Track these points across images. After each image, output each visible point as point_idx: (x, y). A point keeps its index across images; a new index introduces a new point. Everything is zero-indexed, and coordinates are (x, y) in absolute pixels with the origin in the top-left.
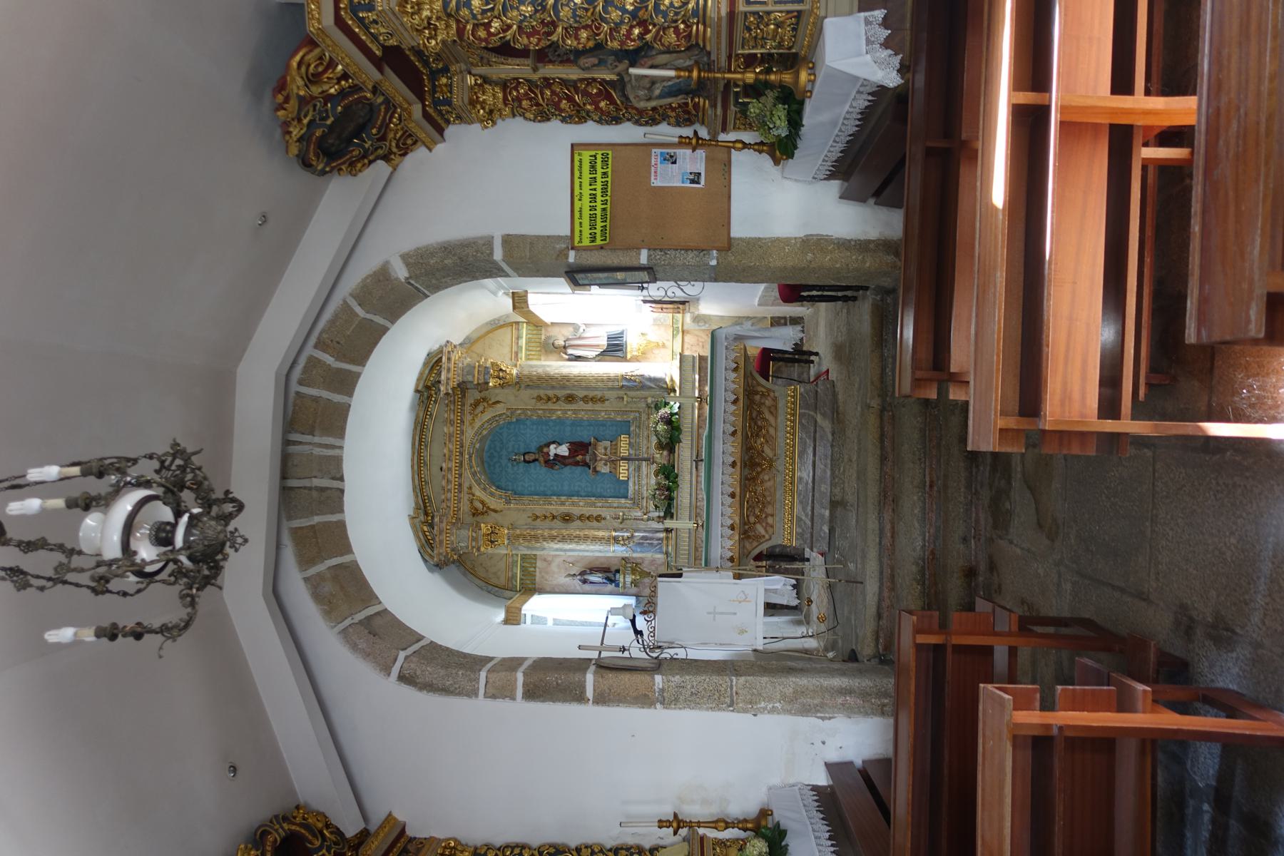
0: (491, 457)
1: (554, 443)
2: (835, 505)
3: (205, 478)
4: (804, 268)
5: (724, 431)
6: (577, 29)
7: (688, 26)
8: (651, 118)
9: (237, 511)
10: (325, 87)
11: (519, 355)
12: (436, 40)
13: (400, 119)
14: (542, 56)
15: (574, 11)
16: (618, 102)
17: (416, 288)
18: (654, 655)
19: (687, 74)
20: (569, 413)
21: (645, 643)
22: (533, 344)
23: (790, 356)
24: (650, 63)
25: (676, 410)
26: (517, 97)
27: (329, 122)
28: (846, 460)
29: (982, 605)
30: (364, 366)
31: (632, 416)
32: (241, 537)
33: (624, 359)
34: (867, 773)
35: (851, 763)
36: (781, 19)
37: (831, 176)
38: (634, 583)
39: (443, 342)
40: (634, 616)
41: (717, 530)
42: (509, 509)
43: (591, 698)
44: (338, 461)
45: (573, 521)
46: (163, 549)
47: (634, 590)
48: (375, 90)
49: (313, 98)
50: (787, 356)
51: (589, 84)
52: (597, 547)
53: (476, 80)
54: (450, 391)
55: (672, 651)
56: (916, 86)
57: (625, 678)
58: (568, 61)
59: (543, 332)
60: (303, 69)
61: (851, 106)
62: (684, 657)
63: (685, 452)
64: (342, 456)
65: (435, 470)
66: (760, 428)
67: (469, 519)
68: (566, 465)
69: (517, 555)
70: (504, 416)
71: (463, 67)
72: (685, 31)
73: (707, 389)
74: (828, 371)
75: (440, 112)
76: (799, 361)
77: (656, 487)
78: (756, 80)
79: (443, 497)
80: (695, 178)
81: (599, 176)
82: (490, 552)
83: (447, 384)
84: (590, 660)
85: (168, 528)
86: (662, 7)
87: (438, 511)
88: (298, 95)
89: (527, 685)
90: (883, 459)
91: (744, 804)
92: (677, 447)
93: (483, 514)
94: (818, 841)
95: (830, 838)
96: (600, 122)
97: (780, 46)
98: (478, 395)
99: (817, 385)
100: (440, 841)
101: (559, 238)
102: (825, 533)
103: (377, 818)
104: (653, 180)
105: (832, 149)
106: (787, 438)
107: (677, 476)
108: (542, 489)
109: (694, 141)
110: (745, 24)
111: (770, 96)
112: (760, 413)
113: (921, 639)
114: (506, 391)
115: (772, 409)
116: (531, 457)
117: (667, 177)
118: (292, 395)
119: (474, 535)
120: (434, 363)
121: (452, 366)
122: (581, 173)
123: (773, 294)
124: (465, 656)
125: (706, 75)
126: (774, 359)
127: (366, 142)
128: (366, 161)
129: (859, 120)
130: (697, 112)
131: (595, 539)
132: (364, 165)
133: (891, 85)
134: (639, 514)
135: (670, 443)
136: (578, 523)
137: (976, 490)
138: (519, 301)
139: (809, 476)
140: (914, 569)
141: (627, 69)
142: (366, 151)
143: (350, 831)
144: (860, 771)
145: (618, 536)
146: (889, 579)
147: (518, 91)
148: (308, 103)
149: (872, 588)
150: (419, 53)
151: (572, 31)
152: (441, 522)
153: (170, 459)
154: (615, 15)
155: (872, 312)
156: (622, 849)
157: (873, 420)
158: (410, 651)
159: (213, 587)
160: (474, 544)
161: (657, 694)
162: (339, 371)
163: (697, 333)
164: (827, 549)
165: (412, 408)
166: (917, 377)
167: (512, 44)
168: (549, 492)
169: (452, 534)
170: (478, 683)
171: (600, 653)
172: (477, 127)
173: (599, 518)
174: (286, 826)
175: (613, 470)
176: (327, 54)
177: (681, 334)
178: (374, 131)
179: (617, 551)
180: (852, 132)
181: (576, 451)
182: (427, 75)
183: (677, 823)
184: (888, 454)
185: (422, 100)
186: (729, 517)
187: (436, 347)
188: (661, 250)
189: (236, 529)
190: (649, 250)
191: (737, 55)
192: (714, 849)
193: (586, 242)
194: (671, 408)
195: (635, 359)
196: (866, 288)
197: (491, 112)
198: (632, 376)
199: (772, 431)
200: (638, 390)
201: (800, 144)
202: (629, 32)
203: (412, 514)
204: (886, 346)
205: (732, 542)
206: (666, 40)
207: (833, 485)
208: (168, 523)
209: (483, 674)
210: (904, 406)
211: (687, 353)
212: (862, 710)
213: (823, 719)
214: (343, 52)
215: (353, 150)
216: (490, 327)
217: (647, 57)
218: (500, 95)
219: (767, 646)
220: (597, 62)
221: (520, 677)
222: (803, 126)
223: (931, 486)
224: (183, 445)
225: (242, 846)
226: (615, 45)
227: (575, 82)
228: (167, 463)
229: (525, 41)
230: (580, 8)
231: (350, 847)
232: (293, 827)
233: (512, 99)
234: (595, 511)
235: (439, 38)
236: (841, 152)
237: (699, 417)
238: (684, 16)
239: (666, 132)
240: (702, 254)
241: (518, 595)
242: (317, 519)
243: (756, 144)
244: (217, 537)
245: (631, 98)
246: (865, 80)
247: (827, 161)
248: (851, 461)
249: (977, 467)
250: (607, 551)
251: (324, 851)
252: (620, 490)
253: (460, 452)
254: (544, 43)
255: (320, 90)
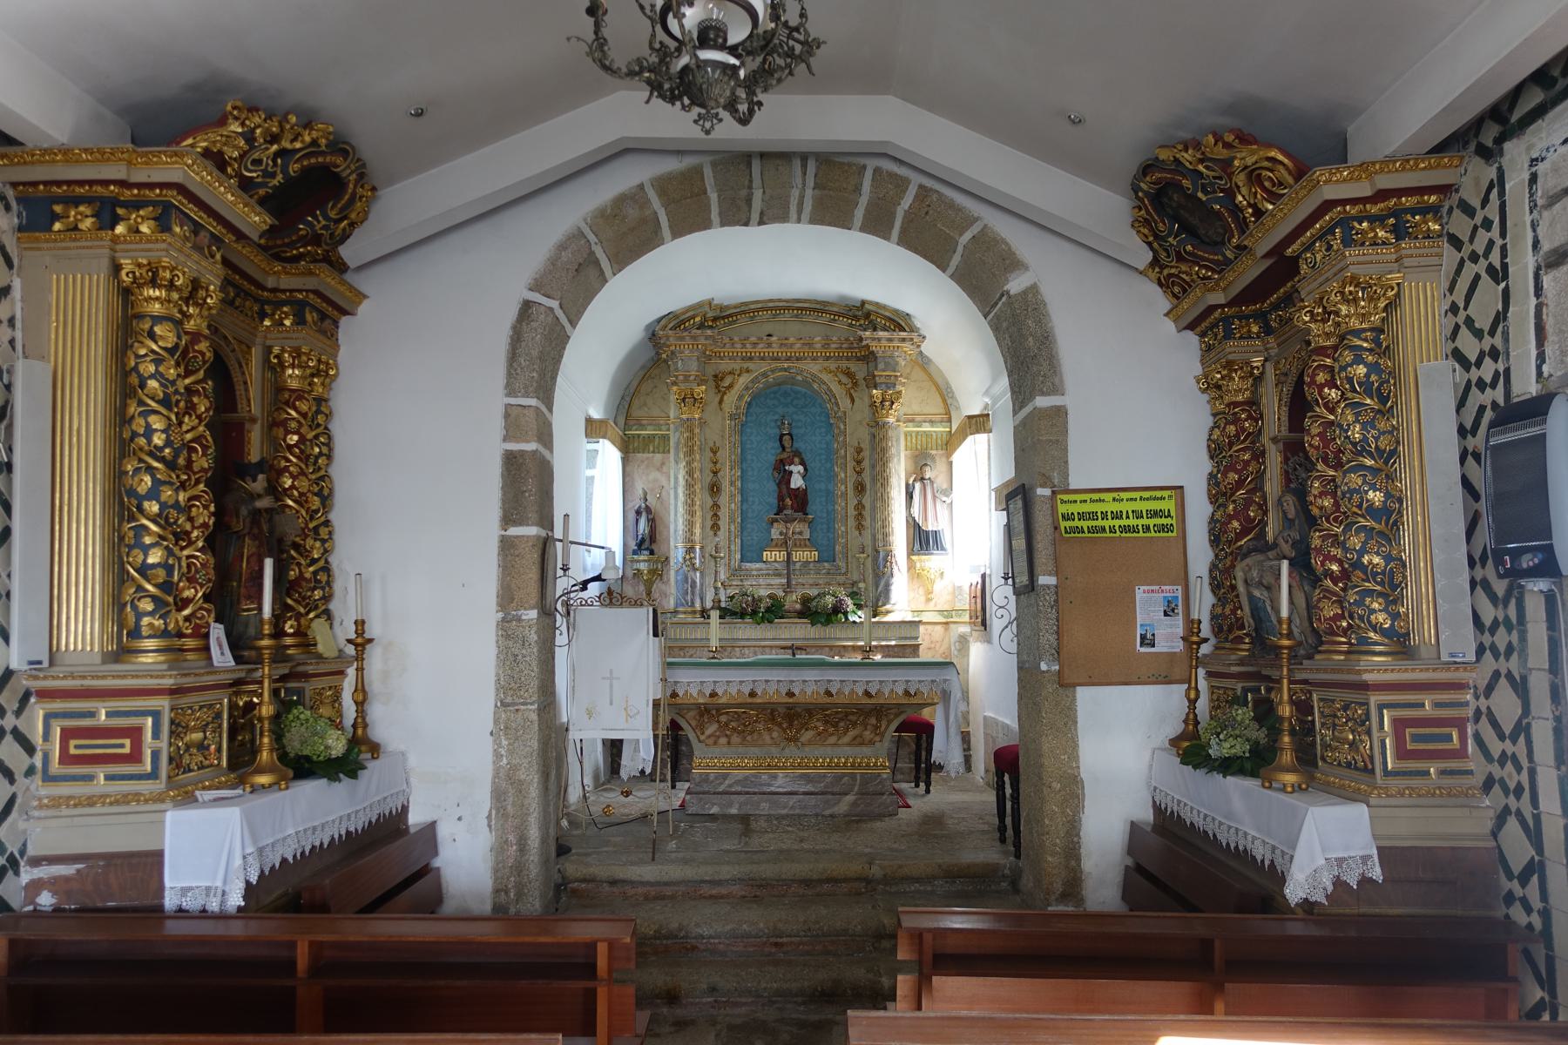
0: (786, 394)
1: (806, 469)
2: (745, 819)
3: (779, 80)
4: (1041, 779)
5: (831, 681)
6: (1334, 494)
7: (1345, 632)
8: (1221, 581)
9: (740, 118)
10: (1244, 190)
11: (911, 424)
12: (1310, 322)
13: (1205, 278)
14: (1293, 448)
15: (1357, 491)
16: (1239, 544)
17: (996, 304)
18: (559, 606)
19: (1285, 632)
20: (843, 487)
21: (572, 595)
22: (924, 439)
23: (923, 758)
24: (1294, 584)
25: (852, 618)
26: (1240, 419)
27: (1200, 195)
28: (801, 834)
29: (643, 1017)
30: (898, 244)
31: (841, 564)
32: (712, 127)
33: (911, 552)
34: (426, 874)
35: (436, 853)
36: (1361, 748)
37: (1158, 810)
38: (638, 573)
39: (923, 332)
40: (604, 580)
41: (710, 677)
42: (724, 419)
43: (508, 533)
44: (783, 218)
45: (712, 496)
46: (695, 36)
47: (630, 573)
48: (1241, 248)
49: (1230, 176)
50: (924, 753)
51: (1260, 506)
52: (681, 527)
53: (1258, 368)
54: (864, 343)
55: (564, 628)
56: (1289, 924)
57: (533, 574)
58: (1288, 480)
59: (940, 452)
60: (1266, 164)
61: (1254, 838)
62: (557, 644)
63: (799, 631)
64: (788, 222)
65: (768, 328)
66: (836, 725)
67: (710, 371)
68: (779, 485)
69: (668, 430)
70: (836, 409)
71: (1273, 352)
72: (1338, 627)
73: (878, 658)
74: (909, 807)
75: (1215, 325)
76: (918, 768)
77: (756, 596)
78: (1281, 719)
79: (736, 339)
80: (1148, 641)
81: (1145, 521)
82: (671, 397)
83: (874, 339)
84: (552, 530)
85: (720, 40)
86: (1368, 600)
87: (719, 333)
88: (1235, 158)
89: (522, 456)
90: (807, 883)
91: (384, 725)
92: (806, 620)
93: (717, 387)
94: (346, 818)
95: (348, 833)
96: (1212, 520)
97: (1326, 746)
98: (860, 376)
99: (891, 794)
100: (335, 356)
101: (1065, 475)
102: (710, 809)
103: (362, 282)
104: (1142, 588)
105: (1195, 812)
106: (824, 759)
107: (770, 622)
108: (749, 457)
109: (1195, 639)
110: (1352, 702)
111: (1261, 735)
112: (854, 724)
113: (602, 949)
114: (867, 412)
115: (859, 740)
116: (787, 443)
117: (1148, 605)
118: (862, 161)
119: (692, 378)
120: (898, 323)
121: (896, 344)
122: (1148, 499)
123: (1001, 735)
124: (554, 378)
125: (1285, 656)
126: (918, 739)
127: (1175, 238)
128: (1151, 239)
129: (1237, 847)
130: (1232, 641)
131: (690, 525)
132: (1146, 236)
133: (1287, 891)
134: (722, 576)
135: (810, 612)
136: (710, 502)
137: (775, 1002)
138: (978, 423)
139: (778, 787)
140: (674, 925)
141: (1285, 558)
142: (1164, 239)
143: (346, 252)
144: (427, 865)
145: (694, 552)
146: (659, 894)
147: (1246, 420)
148: (1224, 170)
149: (647, 872)
150: (1290, 300)
151: (1331, 488)
152: (707, 338)
153: (801, 38)
154: (1356, 542)
155: (988, 865)
156: (329, 576)
157: (854, 868)
158: (559, 313)
159: (648, 93)
160: (681, 378)
161: (514, 613)
162: (892, 216)
163: (946, 641)
164: (690, 812)
165: (843, 298)
166: (925, 935)
167: (1309, 414)
168: (744, 466)
169: (691, 352)
170: (523, 397)
171: (561, 541)
172: (1198, 369)
173: (715, 527)
174: (353, 177)
175: (774, 543)
176: (1285, 191)
177: (944, 620)
178: (1189, 248)
179: (677, 552)
180: (1219, 838)
181: (796, 496)
182: (1261, 308)
183: (362, 642)
184: (814, 888)
185: (1230, 304)
186: (726, 691)
187: (918, 324)
188: (1056, 601)
189: (721, 120)
190: (1056, 587)
191: (1310, 692)
192: (330, 688)
193: (1062, 509)
194: (854, 612)
195: (911, 566)
196: (1018, 856)
197: (1218, 387)
198: (891, 563)
199: (833, 740)
200: (874, 570)
201: (1200, 773)
202: (1334, 559)
203: (715, 302)
204: (947, 882)
205: (695, 695)
206: (1325, 604)
207: (769, 818)
208: (725, 40)
209: (533, 402)
210: (873, 907)
211: (922, 628)
212: (500, 865)
213: (489, 817)
214: (1289, 210)
215: (1165, 224)
216: (943, 387)
217: (1301, 580)
218: (1240, 398)
219: (571, 742)
220: (1290, 517)
221: (531, 446)
222: (1224, 777)
223: (776, 944)
224: (818, 52)
225: (331, 129)
226: (1316, 542)
227: (1261, 489)
228: (796, 35)
229: (1315, 431)
230: (1362, 498)
231: (328, 251)
232: (351, 186)
233: (1236, 413)
234: (724, 523)
235: (1312, 325)
236: (1192, 823)
237: (844, 647)
238: (1359, 626)
239: (1203, 603)
240: (1054, 651)
241: (621, 433)
242: (713, 196)
243: (1196, 716)
244: (711, 99)
245: (1248, 561)
246: (1292, 857)
247: (1178, 805)
248: (801, 841)
249: (804, 1003)
250: (676, 539)
251: (324, 223)
252: (751, 553)
253: (791, 357)
254: (1313, 453)
255: (1240, 184)
